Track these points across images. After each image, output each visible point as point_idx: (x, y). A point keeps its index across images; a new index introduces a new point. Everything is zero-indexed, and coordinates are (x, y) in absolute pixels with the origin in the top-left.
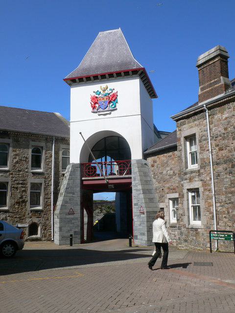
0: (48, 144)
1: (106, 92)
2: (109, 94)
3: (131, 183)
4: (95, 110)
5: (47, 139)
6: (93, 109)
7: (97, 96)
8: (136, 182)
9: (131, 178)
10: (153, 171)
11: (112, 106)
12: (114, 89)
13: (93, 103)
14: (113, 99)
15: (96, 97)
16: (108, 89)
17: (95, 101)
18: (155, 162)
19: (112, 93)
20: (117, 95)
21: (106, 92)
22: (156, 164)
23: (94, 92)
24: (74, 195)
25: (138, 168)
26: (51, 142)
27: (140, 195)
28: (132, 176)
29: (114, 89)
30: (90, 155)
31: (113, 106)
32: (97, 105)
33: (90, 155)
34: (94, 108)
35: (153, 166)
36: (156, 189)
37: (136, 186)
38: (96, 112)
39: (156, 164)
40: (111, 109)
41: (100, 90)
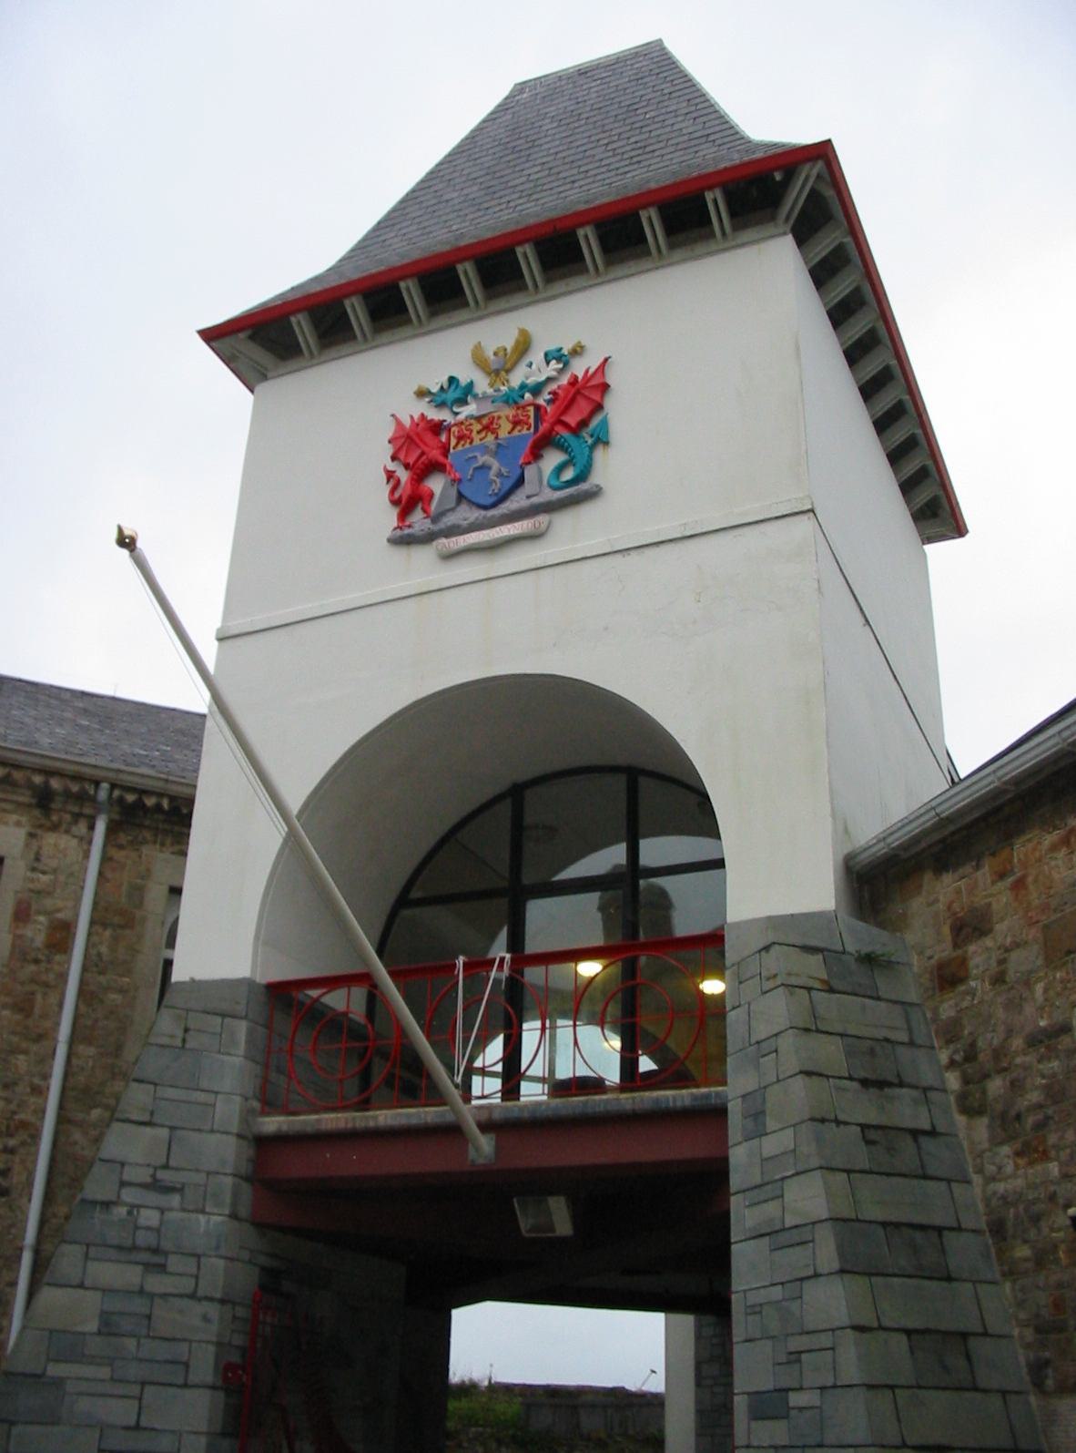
0: (50, 839)
1: (516, 379)
2: (537, 390)
3: (713, 1176)
4: (418, 520)
5: (44, 799)
6: (403, 515)
7: (444, 415)
8: (771, 1145)
9: (717, 1113)
10: (950, 1033)
11: (560, 469)
12: (578, 351)
13: (404, 475)
14: (569, 417)
15: (437, 428)
16: (537, 357)
17: (421, 455)
18: (970, 926)
19: (564, 380)
20: (605, 387)
21: (516, 379)
22: (980, 956)
23: (422, 393)
24: (156, 1283)
25: (219, 1344)
26: (82, 828)
27: (813, 1291)
28: (737, 1086)
29: (578, 351)
30: (506, 1009)
31: (569, 474)
32: (436, 484)
33: (506, 1009)
34: (407, 503)
35: (949, 977)
36: (998, 1229)
37: (771, 1188)
38: (428, 538)
39: (980, 956)
40: (550, 495)
41: (467, 373)
